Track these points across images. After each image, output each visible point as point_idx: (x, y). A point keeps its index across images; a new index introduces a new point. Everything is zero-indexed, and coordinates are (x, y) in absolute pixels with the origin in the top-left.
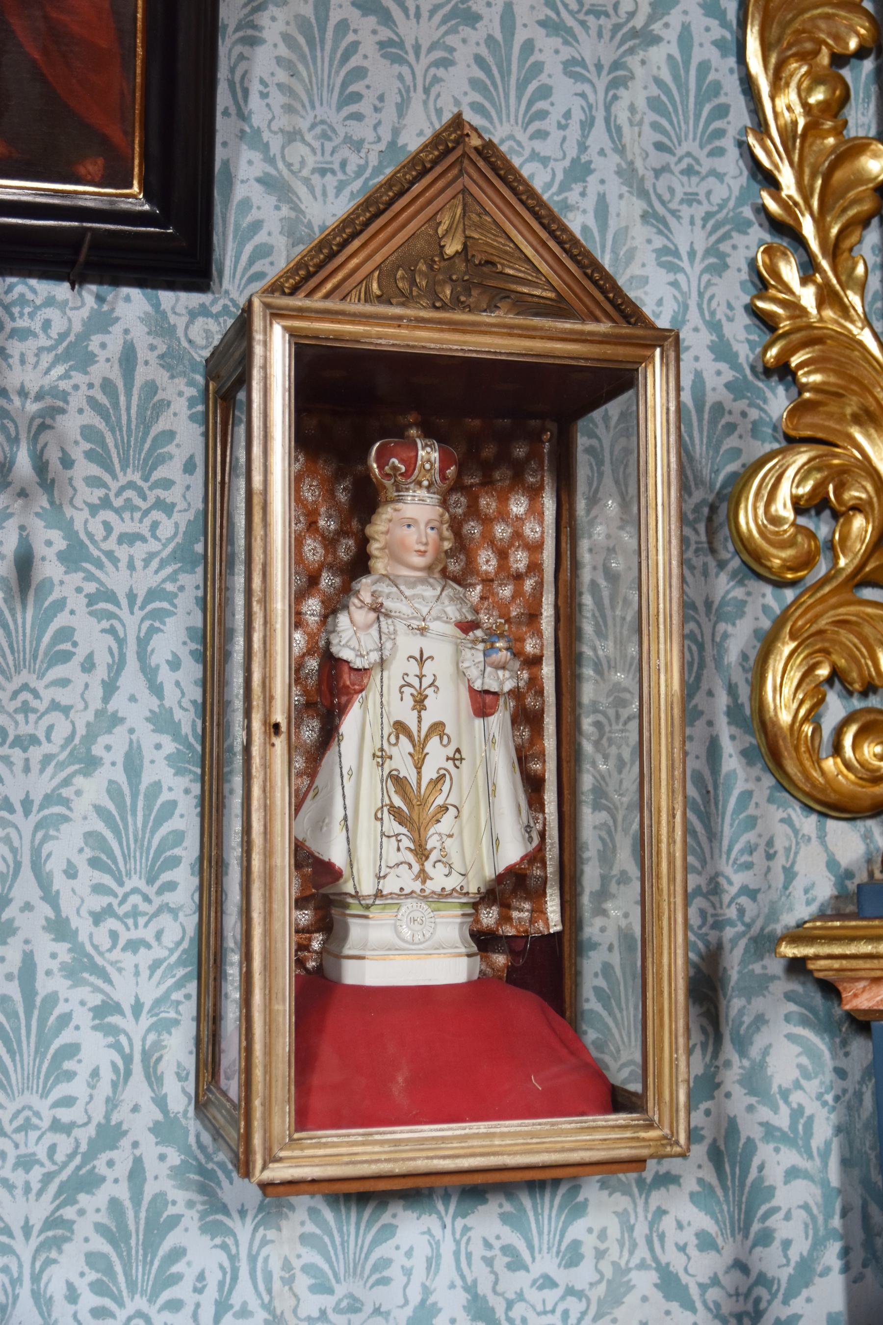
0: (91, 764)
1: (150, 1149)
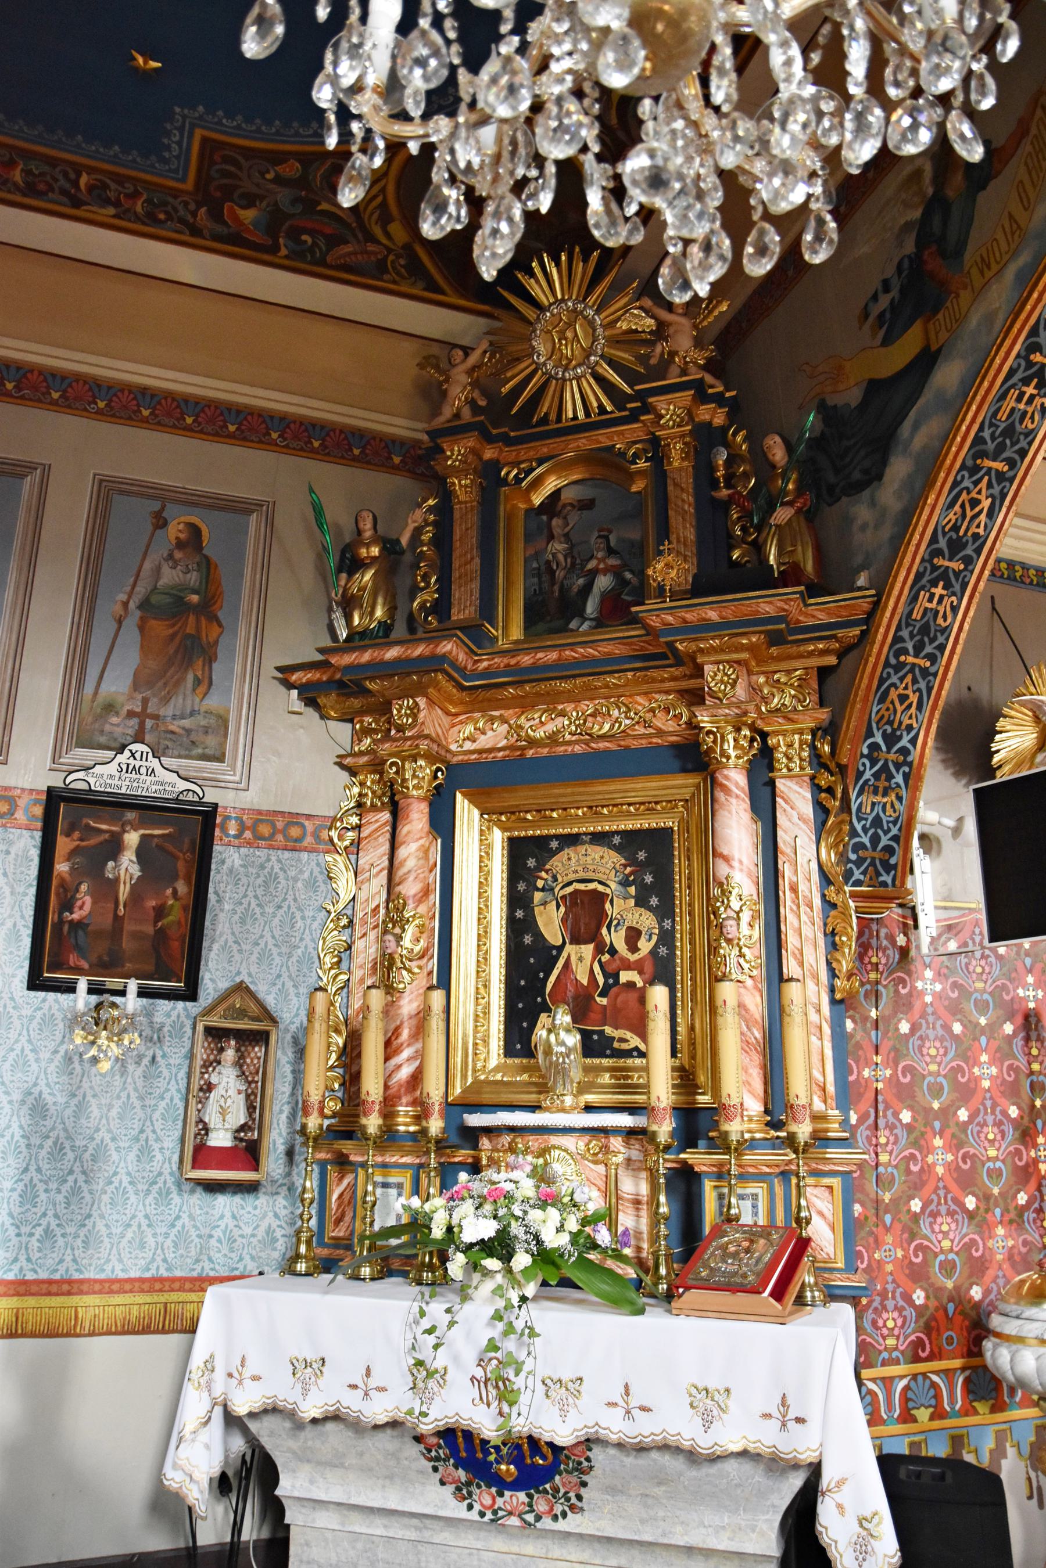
0: (163, 1099)
1: (168, 1177)
